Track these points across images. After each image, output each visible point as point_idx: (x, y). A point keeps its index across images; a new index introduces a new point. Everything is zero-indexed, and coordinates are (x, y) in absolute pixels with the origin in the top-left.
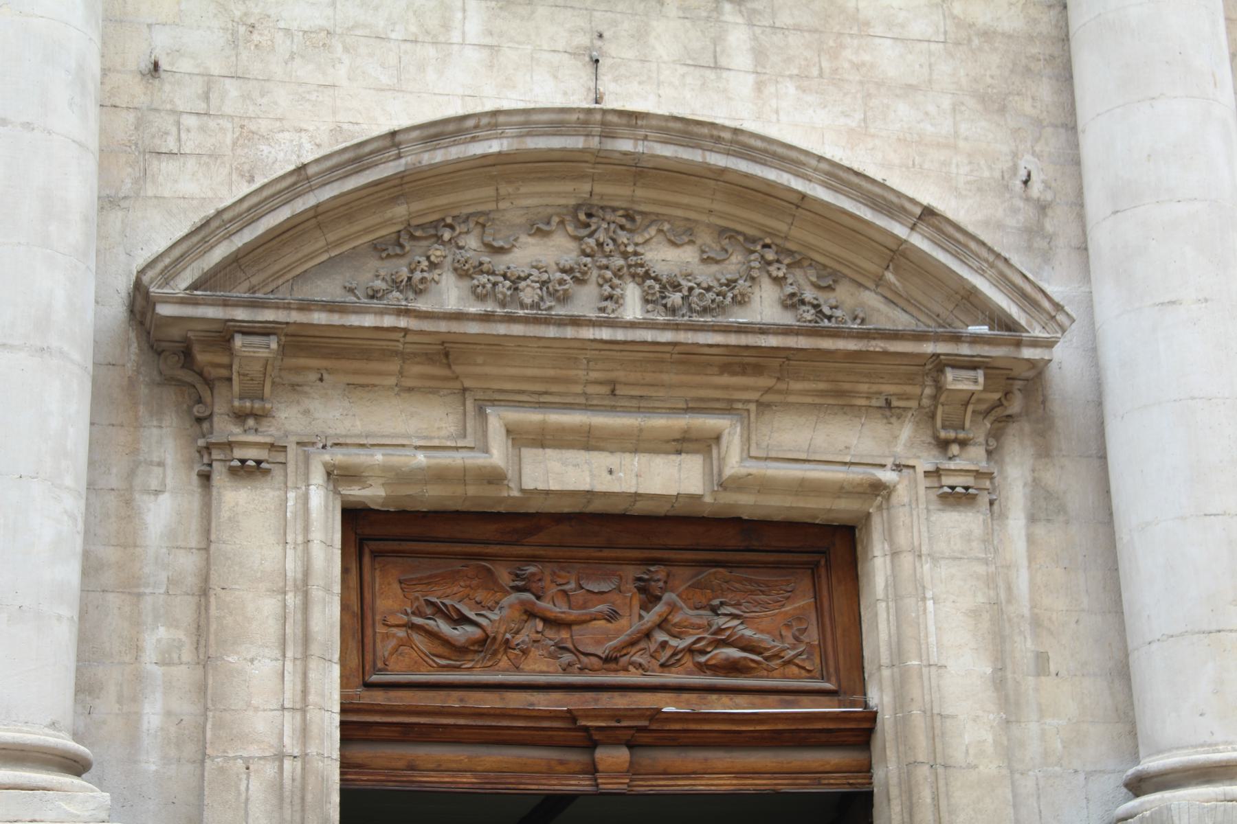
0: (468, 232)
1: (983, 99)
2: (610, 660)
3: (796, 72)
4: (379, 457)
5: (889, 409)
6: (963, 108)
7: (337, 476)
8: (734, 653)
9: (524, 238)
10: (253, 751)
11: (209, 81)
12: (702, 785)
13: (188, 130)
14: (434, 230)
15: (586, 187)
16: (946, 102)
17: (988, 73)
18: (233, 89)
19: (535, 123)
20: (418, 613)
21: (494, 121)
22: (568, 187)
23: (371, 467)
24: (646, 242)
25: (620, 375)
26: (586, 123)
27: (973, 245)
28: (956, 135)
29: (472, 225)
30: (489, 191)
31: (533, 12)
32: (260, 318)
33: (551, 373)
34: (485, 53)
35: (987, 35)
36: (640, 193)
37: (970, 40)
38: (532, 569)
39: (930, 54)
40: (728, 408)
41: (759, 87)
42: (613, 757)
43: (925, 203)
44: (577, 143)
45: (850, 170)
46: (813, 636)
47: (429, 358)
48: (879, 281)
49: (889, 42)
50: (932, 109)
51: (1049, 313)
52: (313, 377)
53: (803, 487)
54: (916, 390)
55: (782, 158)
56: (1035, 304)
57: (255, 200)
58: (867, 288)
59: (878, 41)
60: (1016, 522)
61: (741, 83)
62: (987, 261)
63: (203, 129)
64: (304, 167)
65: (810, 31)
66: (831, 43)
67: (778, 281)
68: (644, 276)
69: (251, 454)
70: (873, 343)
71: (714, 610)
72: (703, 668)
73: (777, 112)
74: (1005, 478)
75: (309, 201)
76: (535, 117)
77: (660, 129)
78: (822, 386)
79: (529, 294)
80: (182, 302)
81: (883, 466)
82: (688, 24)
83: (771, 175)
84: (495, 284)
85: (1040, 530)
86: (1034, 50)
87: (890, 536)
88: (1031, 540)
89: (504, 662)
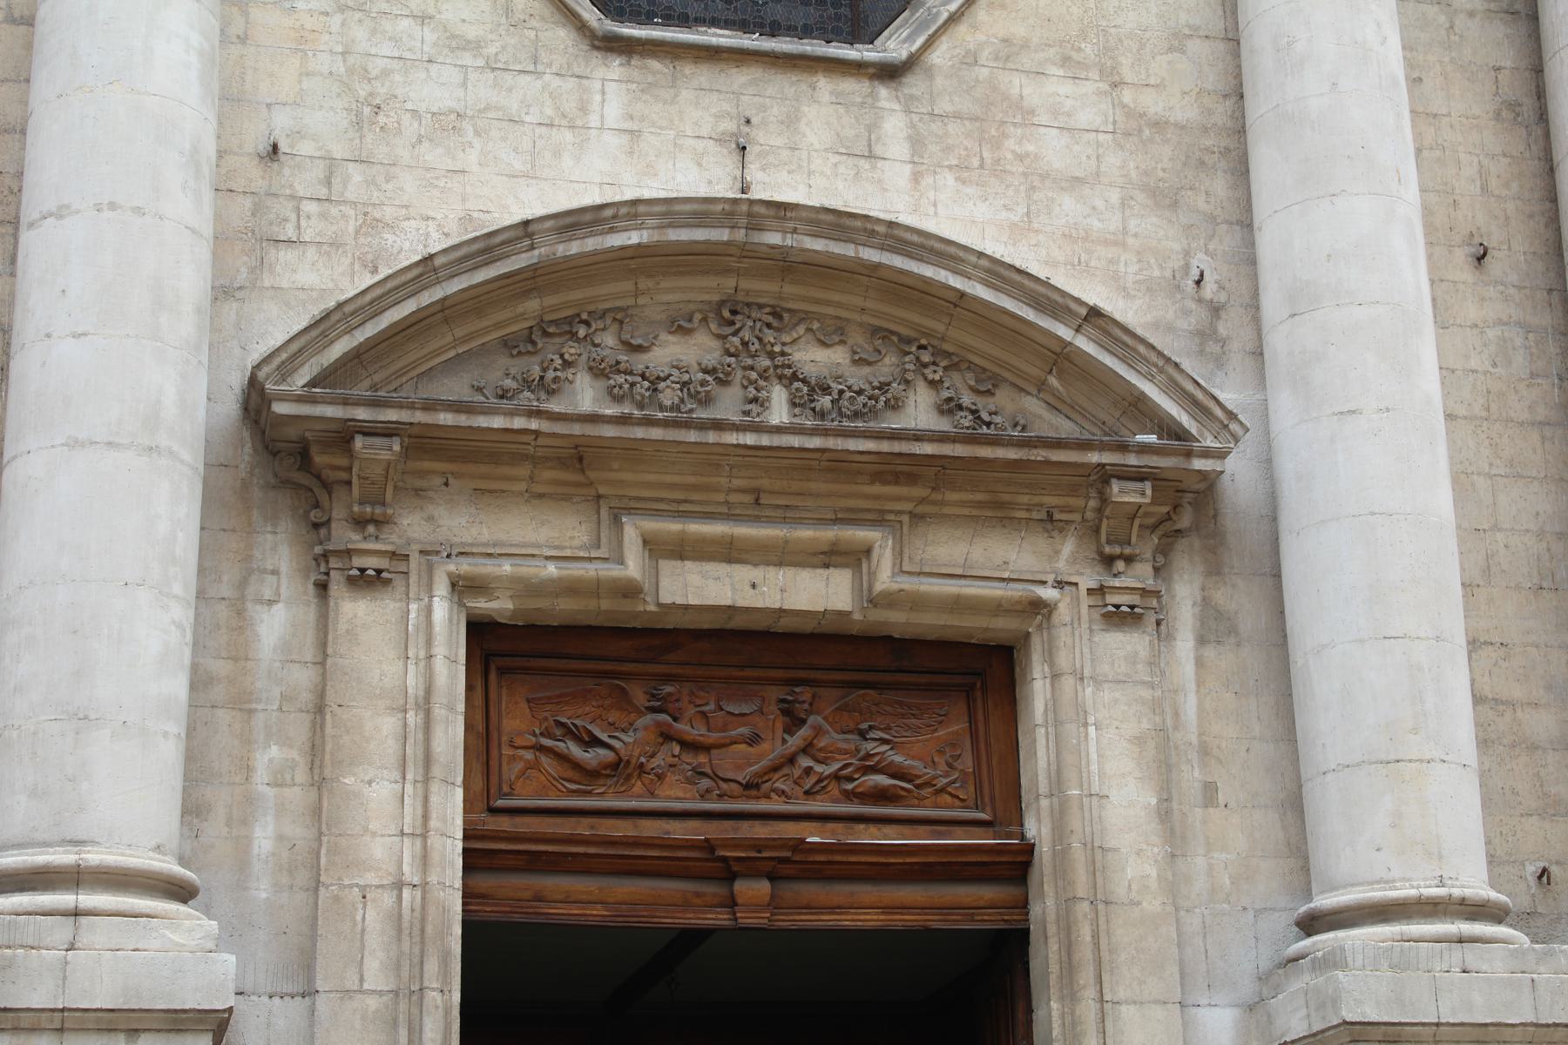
1: (1153, 193)
2: (751, 787)
3: (955, 162)
4: (507, 568)
5: (1051, 523)
7: (462, 587)
8: (883, 780)
9: (664, 336)
10: (371, 878)
12: (847, 921)
13: (309, 217)
14: (569, 326)
15: (730, 283)
16: (1115, 196)
17: (1159, 166)
18: (356, 174)
20: (547, 734)
22: (711, 282)
23: (498, 578)
24: (794, 341)
25: (765, 483)
26: (731, 214)
28: (1125, 231)
30: (627, 286)
31: (676, 96)
33: (691, 480)
34: (625, 138)
35: (1158, 125)
36: (788, 289)
37: (1140, 131)
38: (668, 689)
39: (1099, 145)
40: (879, 519)
41: (916, 178)
42: (753, 890)
43: (1091, 303)
44: (723, 235)
46: (967, 762)
47: (561, 463)
48: (1042, 386)
50: (1099, 203)
51: (1222, 422)
52: (438, 481)
53: (957, 604)
54: (1080, 502)
55: (939, 254)
56: (1206, 412)
57: (378, 291)
58: (1028, 393)
59: (1042, 130)
60: (1185, 644)
61: (897, 174)
62: (1156, 365)
63: (323, 216)
64: (431, 257)
66: (993, 132)
67: (933, 384)
68: (791, 377)
69: (372, 562)
70: (1035, 451)
71: (863, 735)
72: (849, 796)
73: (935, 205)
75: (437, 293)
76: (678, 208)
77: (810, 222)
78: (980, 497)
79: (668, 396)
80: (300, 399)
82: (841, 110)
83: (928, 271)
85: (1210, 652)
86: (1208, 142)
87: (1050, 657)
89: (638, 787)
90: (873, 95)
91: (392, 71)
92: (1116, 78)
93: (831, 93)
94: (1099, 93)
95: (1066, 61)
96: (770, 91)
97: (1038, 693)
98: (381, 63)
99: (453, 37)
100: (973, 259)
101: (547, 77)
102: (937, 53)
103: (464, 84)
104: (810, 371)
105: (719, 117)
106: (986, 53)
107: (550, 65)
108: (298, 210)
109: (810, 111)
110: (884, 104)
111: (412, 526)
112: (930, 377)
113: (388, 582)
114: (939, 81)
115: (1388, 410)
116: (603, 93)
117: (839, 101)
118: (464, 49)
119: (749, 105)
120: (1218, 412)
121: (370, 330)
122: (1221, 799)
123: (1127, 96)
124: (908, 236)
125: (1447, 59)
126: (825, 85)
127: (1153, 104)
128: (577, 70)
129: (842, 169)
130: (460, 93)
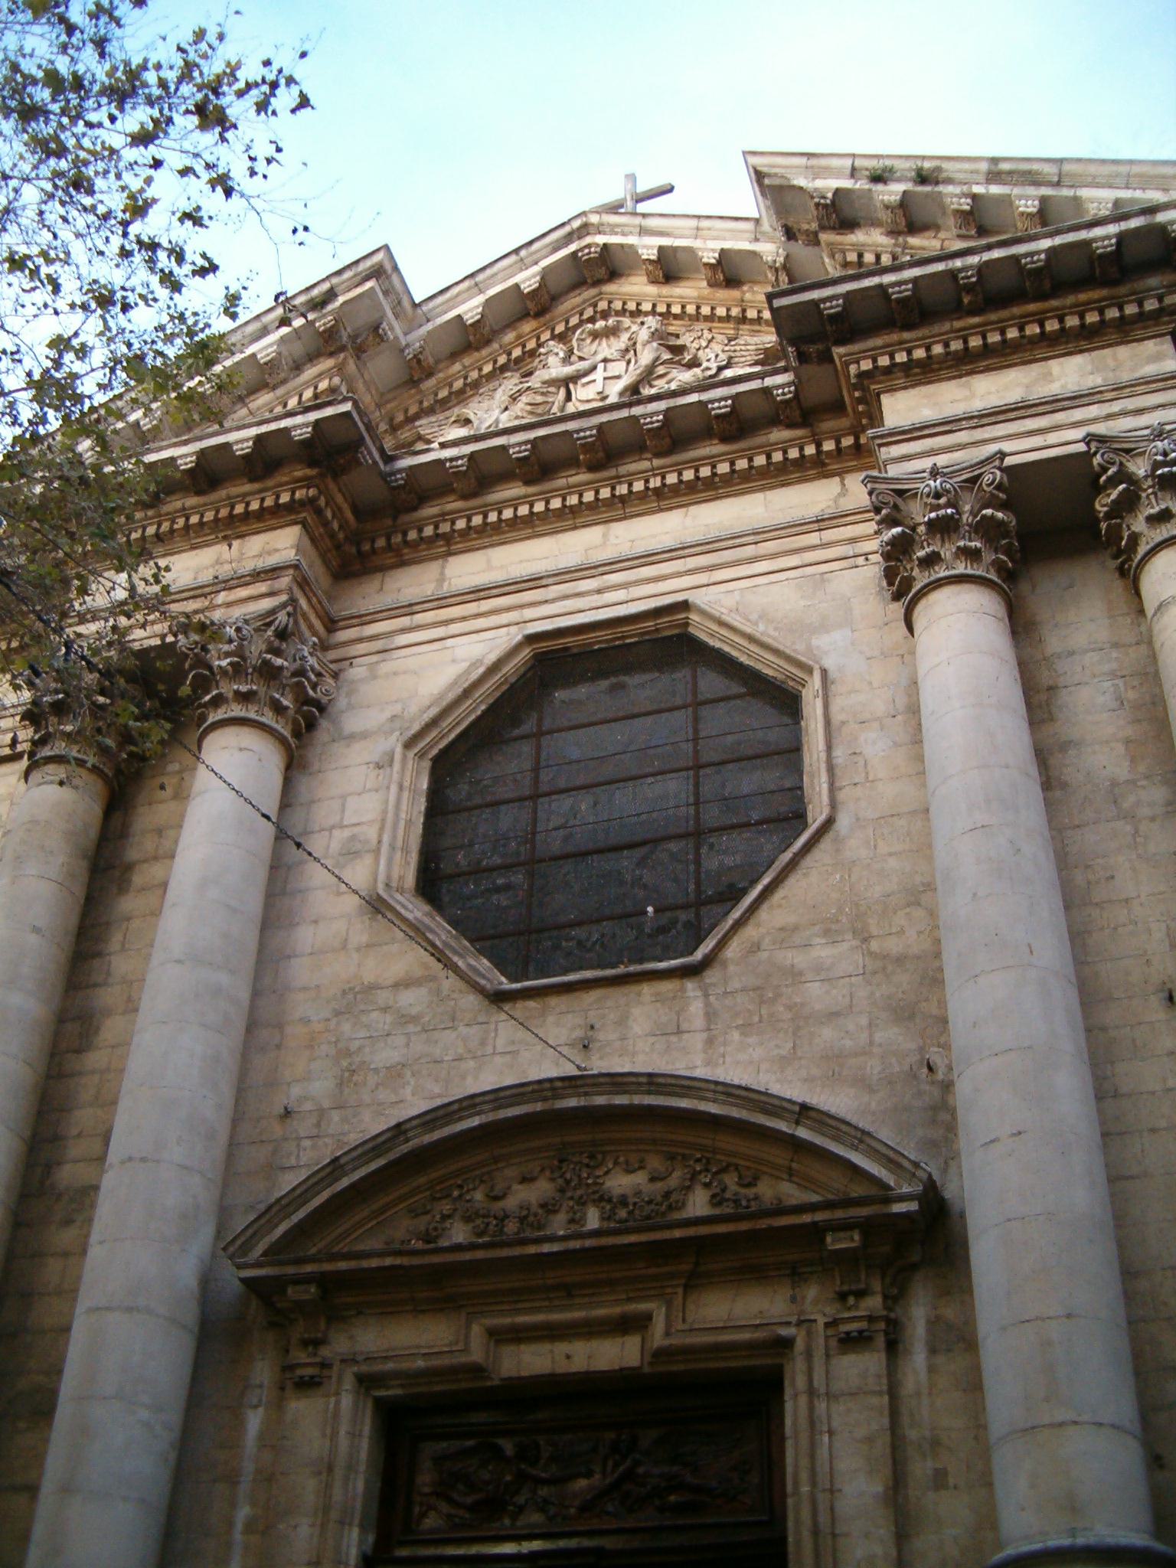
0: (474, 1189)
3: (741, 1022)
6: (878, 1021)
7: (366, 1382)
9: (516, 1187)
11: (322, 1113)
13: (305, 1150)
17: (900, 990)
18: (336, 1116)
19: (502, 1098)
21: (471, 1103)
24: (607, 1173)
27: (844, 1127)
28: (871, 1043)
29: (477, 1183)
31: (544, 1021)
32: (302, 1271)
37: (884, 968)
39: (851, 985)
43: (800, 1100)
45: (739, 1087)
49: (817, 984)
50: (851, 1027)
51: (910, 1172)
56: (899, 1166)
57: (304, 1187)
58: (783, 1179)
59: (808, 985)
62: (855, 1138)
63: (314, 1147)
64: (337, 1159)
65: (754, 990)
66: (770, 995)
67: (707, 1185)
68: (602, 1198)
69: (309, 1371)
70: (760, 1221)
73: (724, 1056)
74: (910, 1319)
75: (345, 1182)
76: (502, 1094)
79: (511, 1227)
81: (788, 1324)
82: (658, 1005)
84: (488, 1224)
85: (940, 1359)
88: (932, 1369)
90: (683, 990)
91: (364, 1047)
92: (866, 935)
93: (652, 995)
94: (853, 949)
95: (827, 932)
96: (609, 1003)
97: (794, 1410)
98: (357, 1043)
99: (403, 1016)
100: (712, 1087)
101: (460, 1029)
102: (731, 949)
103: (408, 1045)
104: (617, 1192)
105: (573, 1029)
106: (767, 940)
107: (462, 1020)
108: (298, 1145)
109: (636, 1011)
110: (691, 994)
111: (339, 1344)
112: (703, 1180)
113: (319, 1384)
114: (732, 968)
115: (1020, 1133)
116: (496, 1030)
117: (659, 998)
118: (409, 1022)
119: (593, 1016)
120: (906, 1164)
121: (301, 1214)
122: (951, 1481)
123: (874, 945)
124: (661, 1080)
125: (1134, 857)
126: (647, 989)
127: (894, 946)
128: (480, 1019)
129: (657, 1046)
130: (405, 1051)
